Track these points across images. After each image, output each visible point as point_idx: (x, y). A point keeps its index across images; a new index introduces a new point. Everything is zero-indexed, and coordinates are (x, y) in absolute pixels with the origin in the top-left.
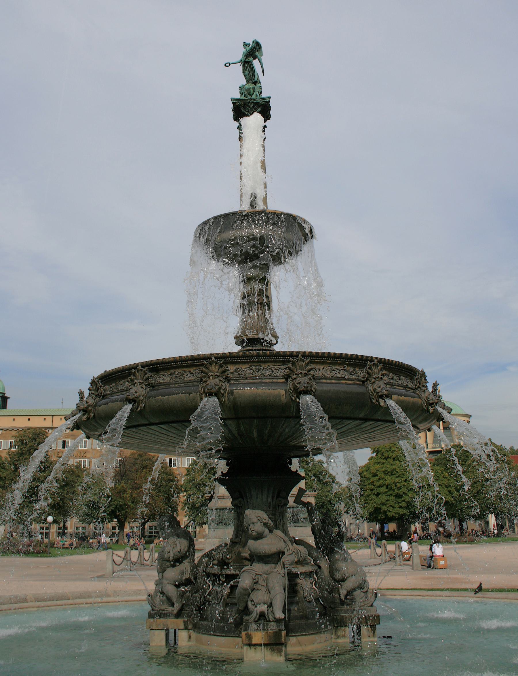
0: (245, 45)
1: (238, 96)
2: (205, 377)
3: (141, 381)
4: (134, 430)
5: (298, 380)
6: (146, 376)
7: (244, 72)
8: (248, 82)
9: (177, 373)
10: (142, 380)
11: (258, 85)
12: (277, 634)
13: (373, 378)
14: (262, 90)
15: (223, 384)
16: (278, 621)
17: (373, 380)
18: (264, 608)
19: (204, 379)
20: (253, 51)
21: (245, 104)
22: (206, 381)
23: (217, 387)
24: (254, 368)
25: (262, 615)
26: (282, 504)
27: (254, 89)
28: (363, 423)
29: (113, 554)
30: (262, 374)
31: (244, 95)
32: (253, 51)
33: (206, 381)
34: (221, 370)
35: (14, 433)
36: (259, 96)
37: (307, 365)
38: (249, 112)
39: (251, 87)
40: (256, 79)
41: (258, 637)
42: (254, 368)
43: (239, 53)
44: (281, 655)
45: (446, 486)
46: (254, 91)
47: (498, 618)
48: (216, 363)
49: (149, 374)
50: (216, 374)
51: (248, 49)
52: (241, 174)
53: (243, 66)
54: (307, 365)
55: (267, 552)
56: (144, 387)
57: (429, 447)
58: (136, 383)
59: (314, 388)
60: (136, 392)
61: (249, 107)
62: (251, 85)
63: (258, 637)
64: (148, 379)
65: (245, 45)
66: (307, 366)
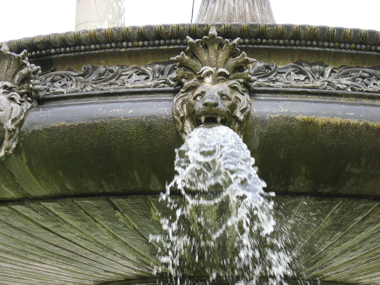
3: (9, 84)
6: (24, 71)
10: (12, 82)
15: (239, 96)
24: (307, 68)
30: (329, 83)
33: (193, 88)
34: (232, 62)
42: (307, 68)
47: (379, 284)
48: (221, 45)
50: (221, 70)
52: (104, 264)
56: (17, 97)
59: (242, 111)
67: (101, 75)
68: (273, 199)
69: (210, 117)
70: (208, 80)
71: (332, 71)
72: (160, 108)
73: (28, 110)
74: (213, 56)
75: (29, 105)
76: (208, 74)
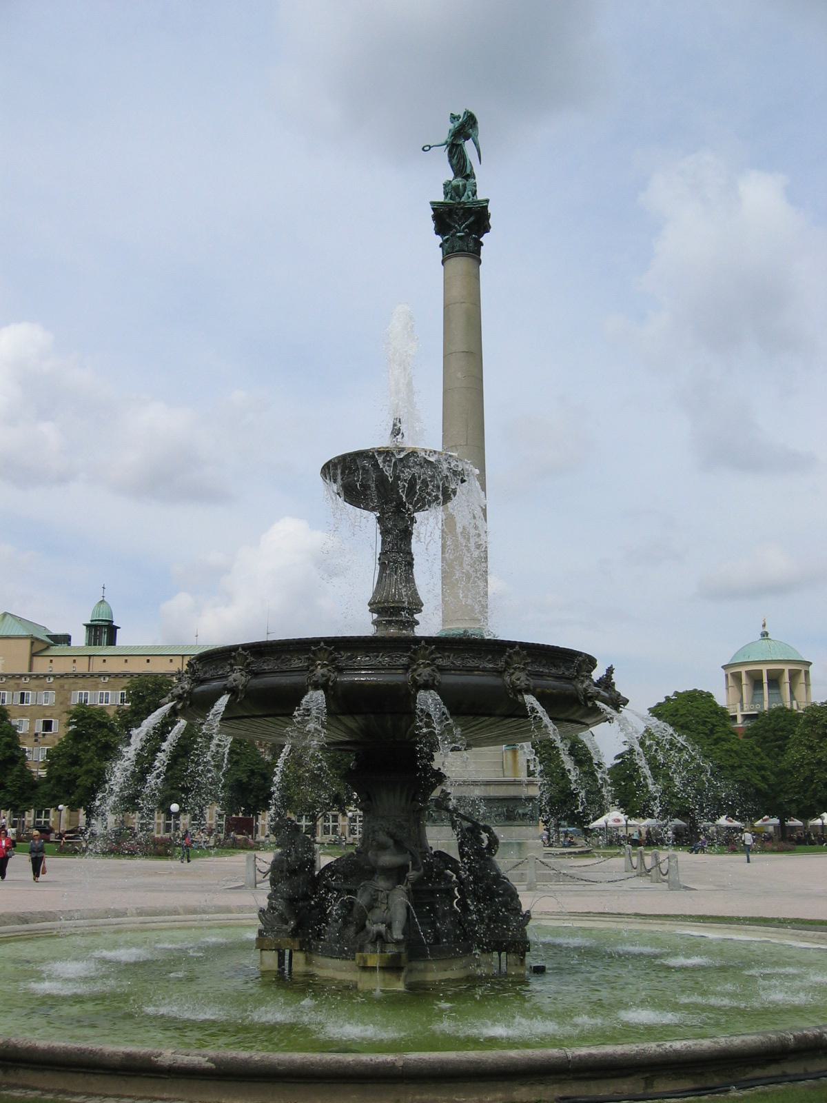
0: (454, 118)
1: (440, 198)
2: (312, 665)
4: (237, 722)
5: (419, 671)
7: (450, 161)
8: (456, 176)
9: (283, 657)
10: (243, 666)
11: (472, 180)
12: (396, 957)
13: (513, 668)
14: (477, 189)
15: (332, 674)
16: (398, 942)
17: (512, 671)
18: (382, 928)
19: (311, 668)
20: (465, 128)
21: (451, 210)
22: (313, 671)
23: (324, 679)
25: (379, 936)
26: (417, 809)
27: (465, 186)
28: (502, 720)
29: (255, 858)
31: (449, 196)
32: (465, 128)
35: (126, 682)
36: (471, 197)
37: (432, 653)
38: (457, 223)
39: (461, 183)
40: (468, 172)
41: (374, 960)
43: (444, 131)
44: (399, 980)
45: (757, 768)
46: (465, 191)
49: (251, 659)
50: (325, 662)
51: (457, 124)
53: (450, 152)
54: (432, 653)
55: (388, 864)
57: (745, 709)
58: (235, 669)
60: (235, 680)
61: (457, 215)
62: (459, 182)
63: (374, 960)
64: (249, 664)
65: (454, 118)
66: (432, 654)
67: (283, 660)
68: (322, 687)
69: (426, 686)
70: (319, 667)
71: (383, 655)
72: (397, 678)
73: (249, 680)
74: (322, 655)
75: (250, 677)
76: (319, 664)
